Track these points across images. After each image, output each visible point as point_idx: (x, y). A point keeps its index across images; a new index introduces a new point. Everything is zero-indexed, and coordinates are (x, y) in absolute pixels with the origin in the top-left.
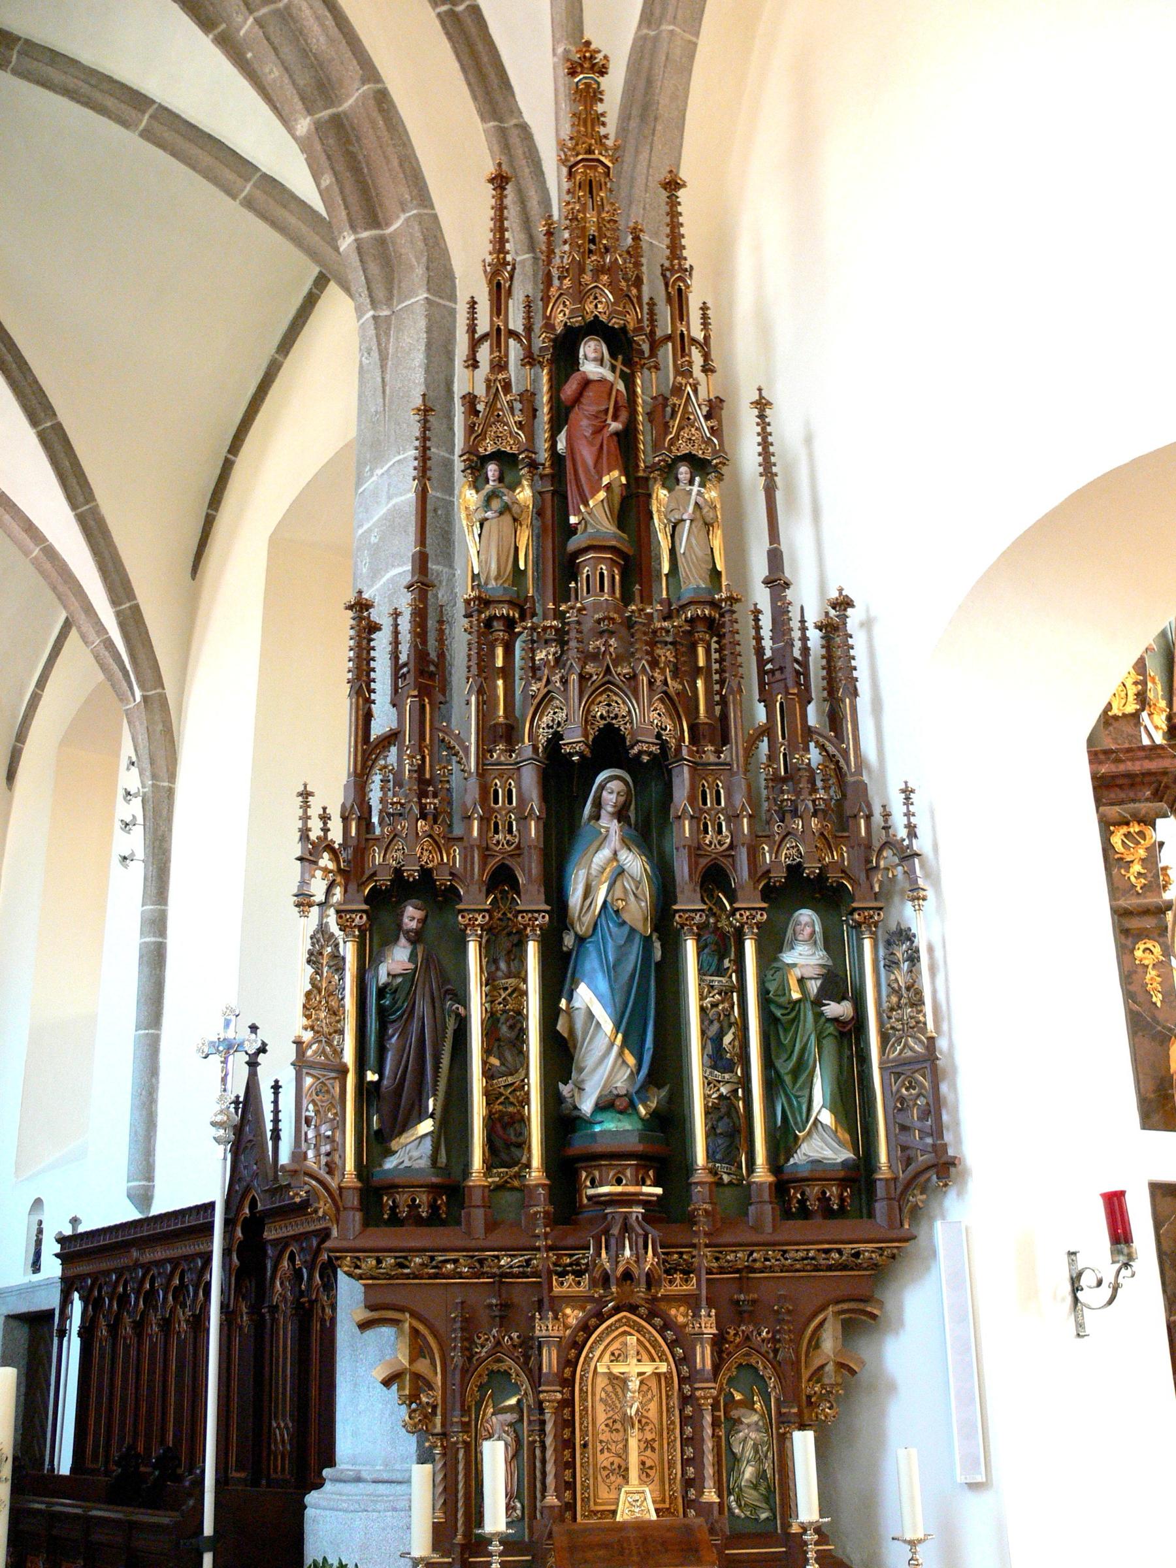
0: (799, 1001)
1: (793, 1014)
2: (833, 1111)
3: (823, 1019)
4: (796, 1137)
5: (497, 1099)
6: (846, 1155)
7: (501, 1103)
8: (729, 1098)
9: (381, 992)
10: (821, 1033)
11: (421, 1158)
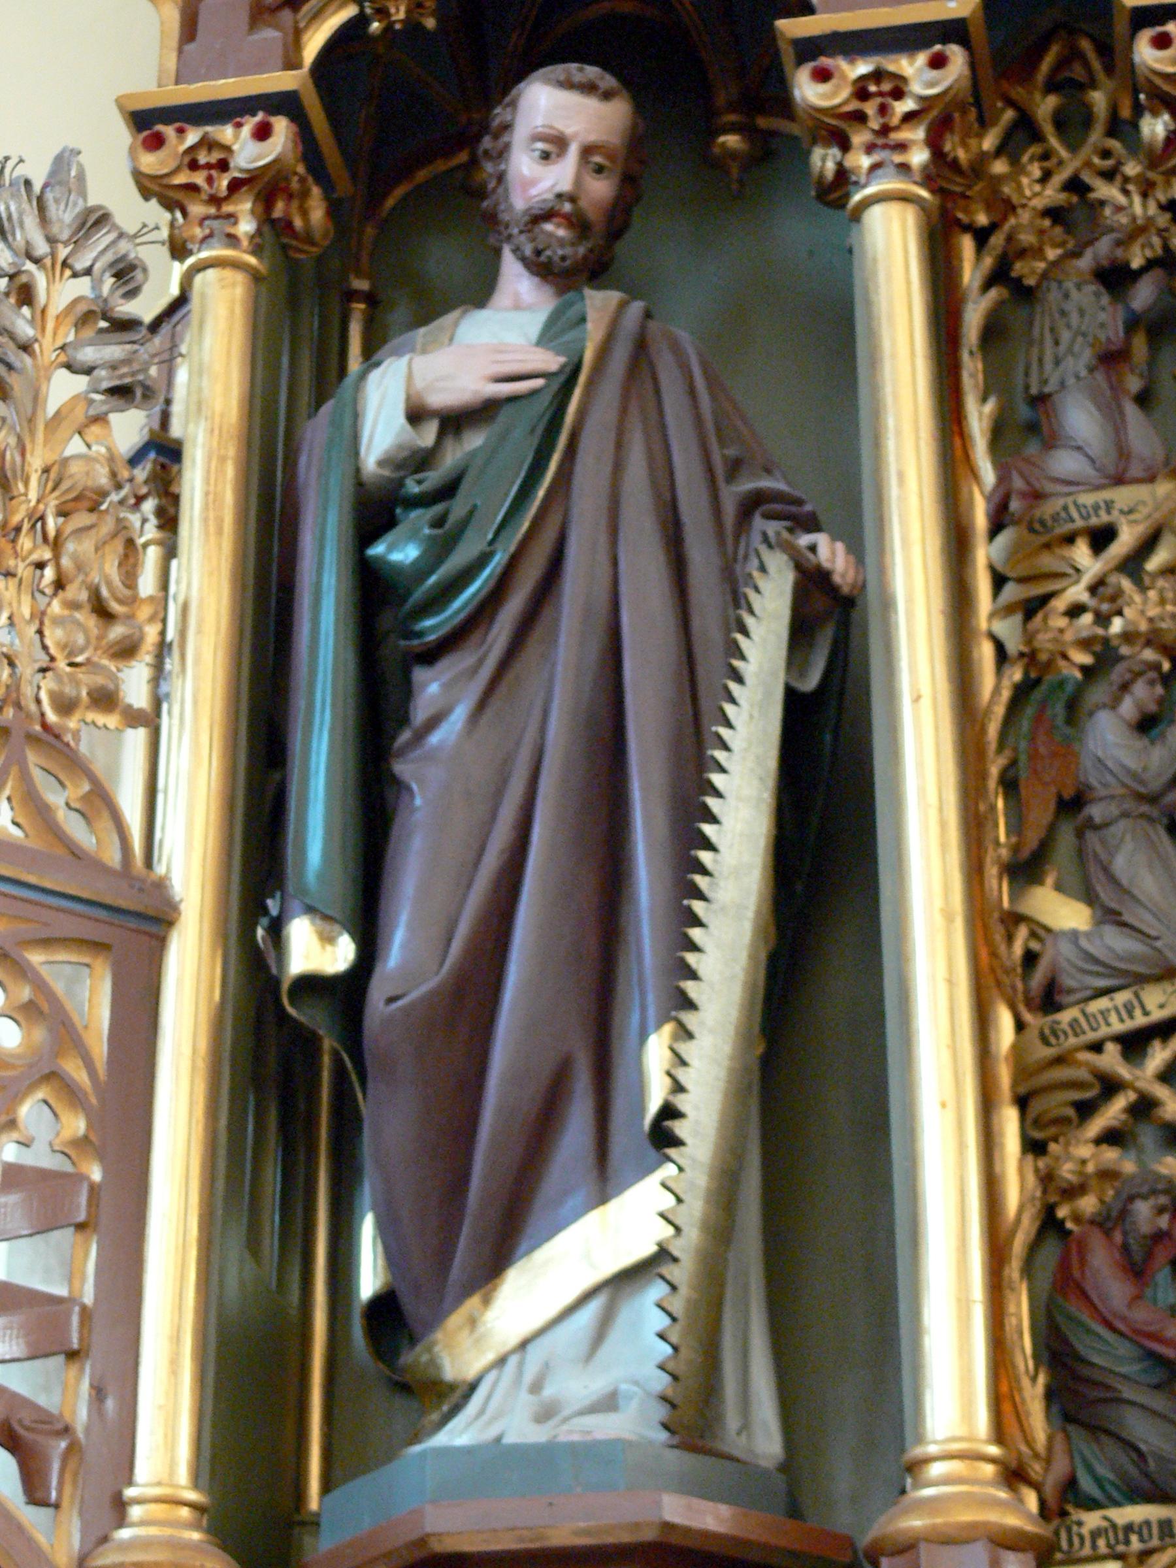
5: (1086, 1110)
7: (1111, 1137)
9: (375, 512)
11: (609, 1403)
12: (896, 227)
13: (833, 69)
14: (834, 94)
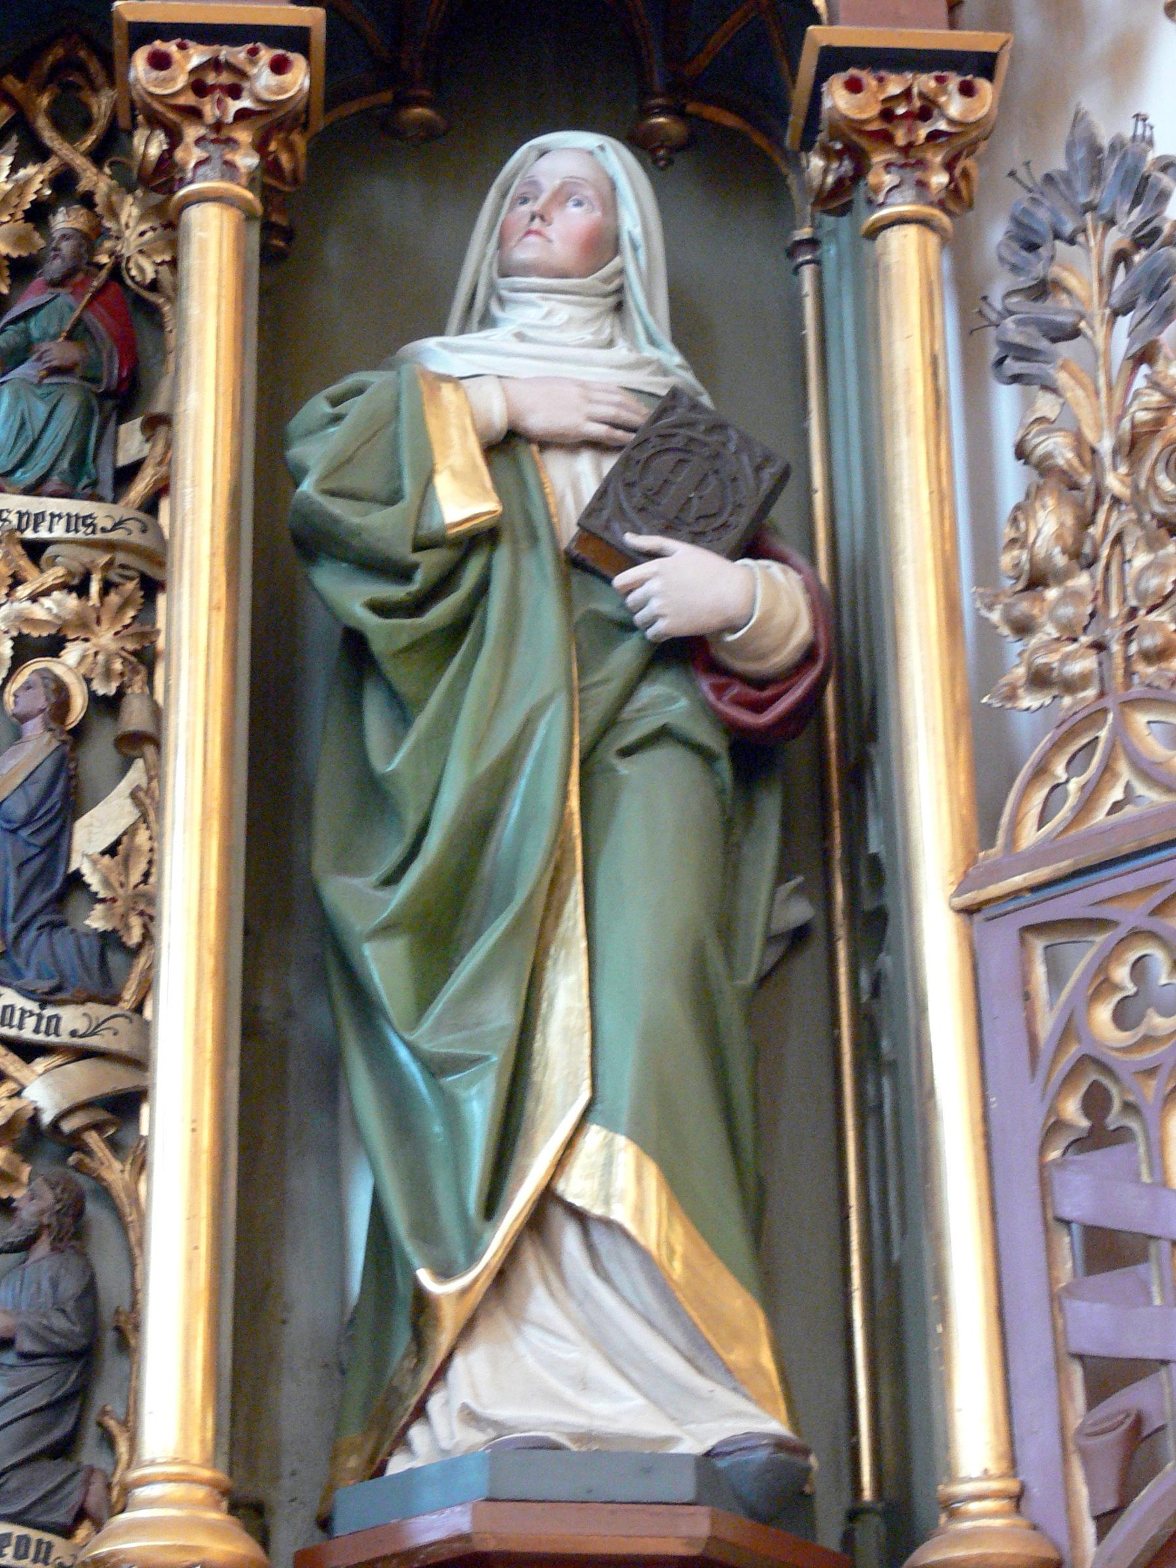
0: (481, 539)
1: (440, 612)
2: (660, 1143)
3: (625, 655)
4: (422, 1302)
6: (734, 1413)
8: (75, 1142)
10: (611, 723)
12: (214, 223)
13: (865, 86)
14: (861, 109)
